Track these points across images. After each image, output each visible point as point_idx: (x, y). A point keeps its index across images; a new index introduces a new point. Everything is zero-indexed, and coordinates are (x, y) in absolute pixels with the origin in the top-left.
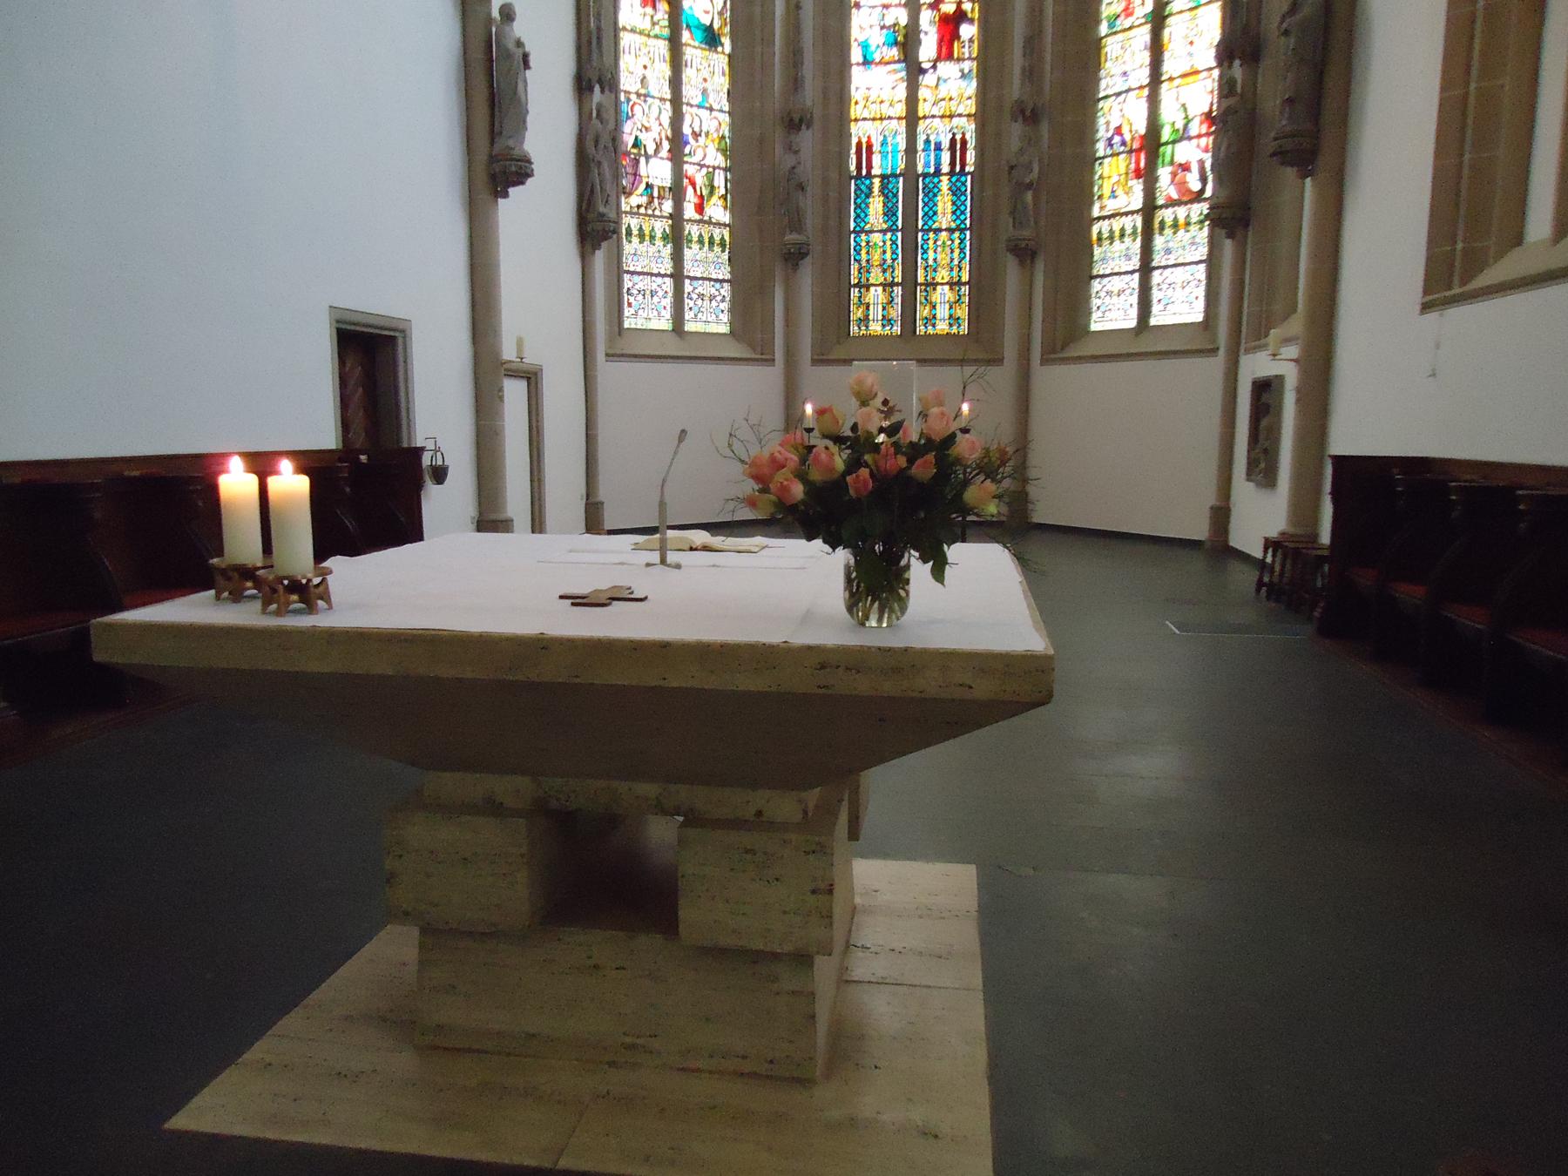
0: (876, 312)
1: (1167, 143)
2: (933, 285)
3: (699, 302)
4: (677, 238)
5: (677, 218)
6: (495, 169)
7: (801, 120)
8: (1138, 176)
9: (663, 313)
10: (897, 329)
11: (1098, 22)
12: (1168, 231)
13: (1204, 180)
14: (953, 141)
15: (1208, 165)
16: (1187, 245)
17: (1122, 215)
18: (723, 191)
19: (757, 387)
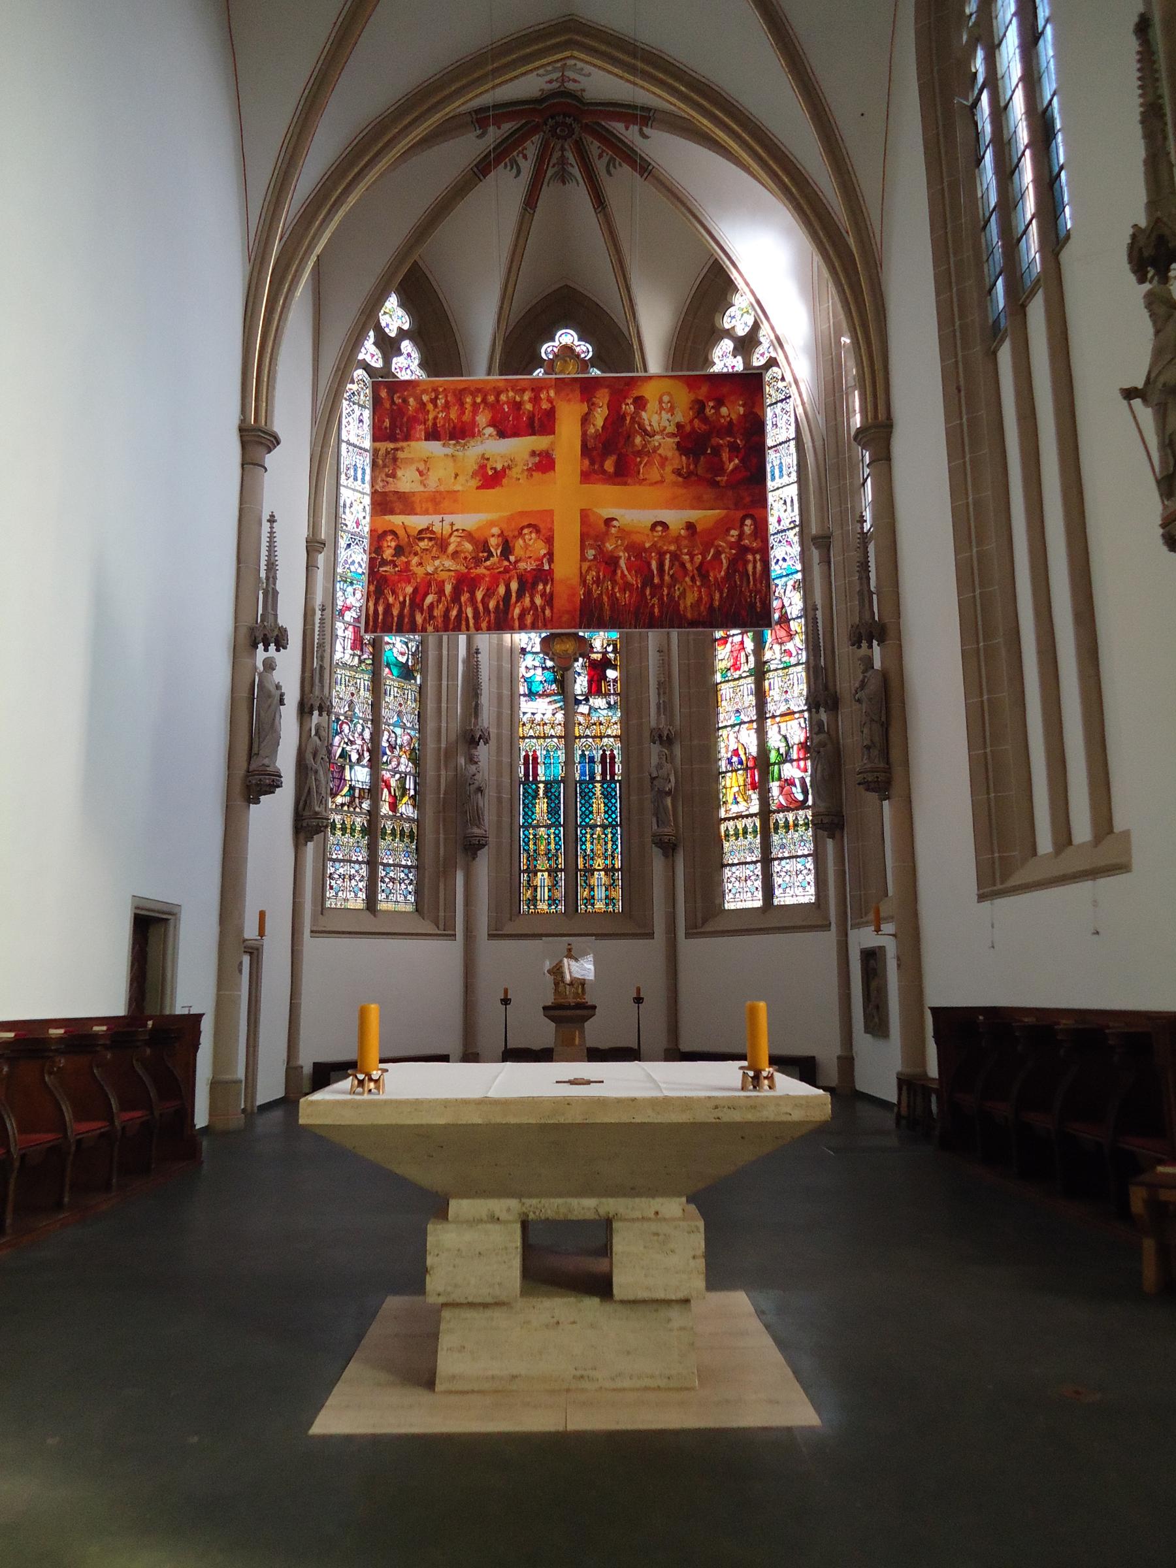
0: (600, 893)
1: (775, 764)
2: (590, 871)
3: (391, 885)
4: (372, 831)
5: (373, 814)
6: (250, 782)
7: (480, 738)
8: (754, 788)
9: (360, 894)
10: (561, 908)
11: (714, 672)
12: (781, 831)
13: (805, 792)
14: (604, 756)
15: (808, 780)
16: (796, 846)
17: (743, 817)
19: (438, 959)
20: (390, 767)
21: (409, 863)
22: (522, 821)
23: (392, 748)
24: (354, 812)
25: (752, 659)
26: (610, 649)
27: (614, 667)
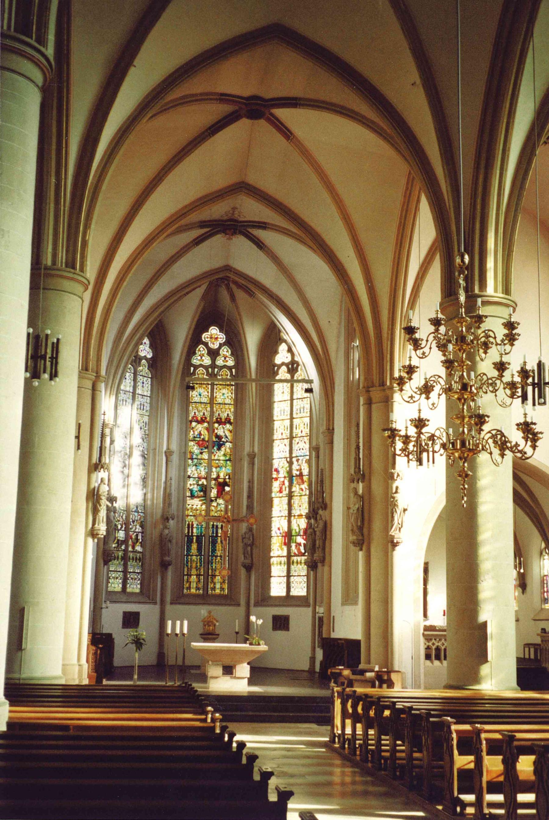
0: (194, 585)
5: (126, 551)
10: (201, 592)
12: (295, 564)
16: (300, 569)
18: (141, 540)
20: (132, 530)
21: (139, 571)
22: (186, 553)
23: (133, 522)
24: (119, 550)
25: (287, 489)
26: (227, 477)
27: (228, 486)
